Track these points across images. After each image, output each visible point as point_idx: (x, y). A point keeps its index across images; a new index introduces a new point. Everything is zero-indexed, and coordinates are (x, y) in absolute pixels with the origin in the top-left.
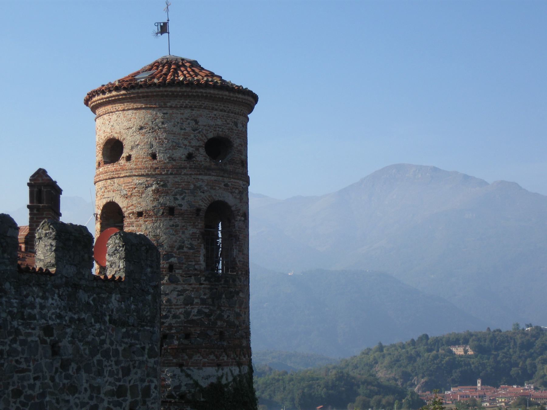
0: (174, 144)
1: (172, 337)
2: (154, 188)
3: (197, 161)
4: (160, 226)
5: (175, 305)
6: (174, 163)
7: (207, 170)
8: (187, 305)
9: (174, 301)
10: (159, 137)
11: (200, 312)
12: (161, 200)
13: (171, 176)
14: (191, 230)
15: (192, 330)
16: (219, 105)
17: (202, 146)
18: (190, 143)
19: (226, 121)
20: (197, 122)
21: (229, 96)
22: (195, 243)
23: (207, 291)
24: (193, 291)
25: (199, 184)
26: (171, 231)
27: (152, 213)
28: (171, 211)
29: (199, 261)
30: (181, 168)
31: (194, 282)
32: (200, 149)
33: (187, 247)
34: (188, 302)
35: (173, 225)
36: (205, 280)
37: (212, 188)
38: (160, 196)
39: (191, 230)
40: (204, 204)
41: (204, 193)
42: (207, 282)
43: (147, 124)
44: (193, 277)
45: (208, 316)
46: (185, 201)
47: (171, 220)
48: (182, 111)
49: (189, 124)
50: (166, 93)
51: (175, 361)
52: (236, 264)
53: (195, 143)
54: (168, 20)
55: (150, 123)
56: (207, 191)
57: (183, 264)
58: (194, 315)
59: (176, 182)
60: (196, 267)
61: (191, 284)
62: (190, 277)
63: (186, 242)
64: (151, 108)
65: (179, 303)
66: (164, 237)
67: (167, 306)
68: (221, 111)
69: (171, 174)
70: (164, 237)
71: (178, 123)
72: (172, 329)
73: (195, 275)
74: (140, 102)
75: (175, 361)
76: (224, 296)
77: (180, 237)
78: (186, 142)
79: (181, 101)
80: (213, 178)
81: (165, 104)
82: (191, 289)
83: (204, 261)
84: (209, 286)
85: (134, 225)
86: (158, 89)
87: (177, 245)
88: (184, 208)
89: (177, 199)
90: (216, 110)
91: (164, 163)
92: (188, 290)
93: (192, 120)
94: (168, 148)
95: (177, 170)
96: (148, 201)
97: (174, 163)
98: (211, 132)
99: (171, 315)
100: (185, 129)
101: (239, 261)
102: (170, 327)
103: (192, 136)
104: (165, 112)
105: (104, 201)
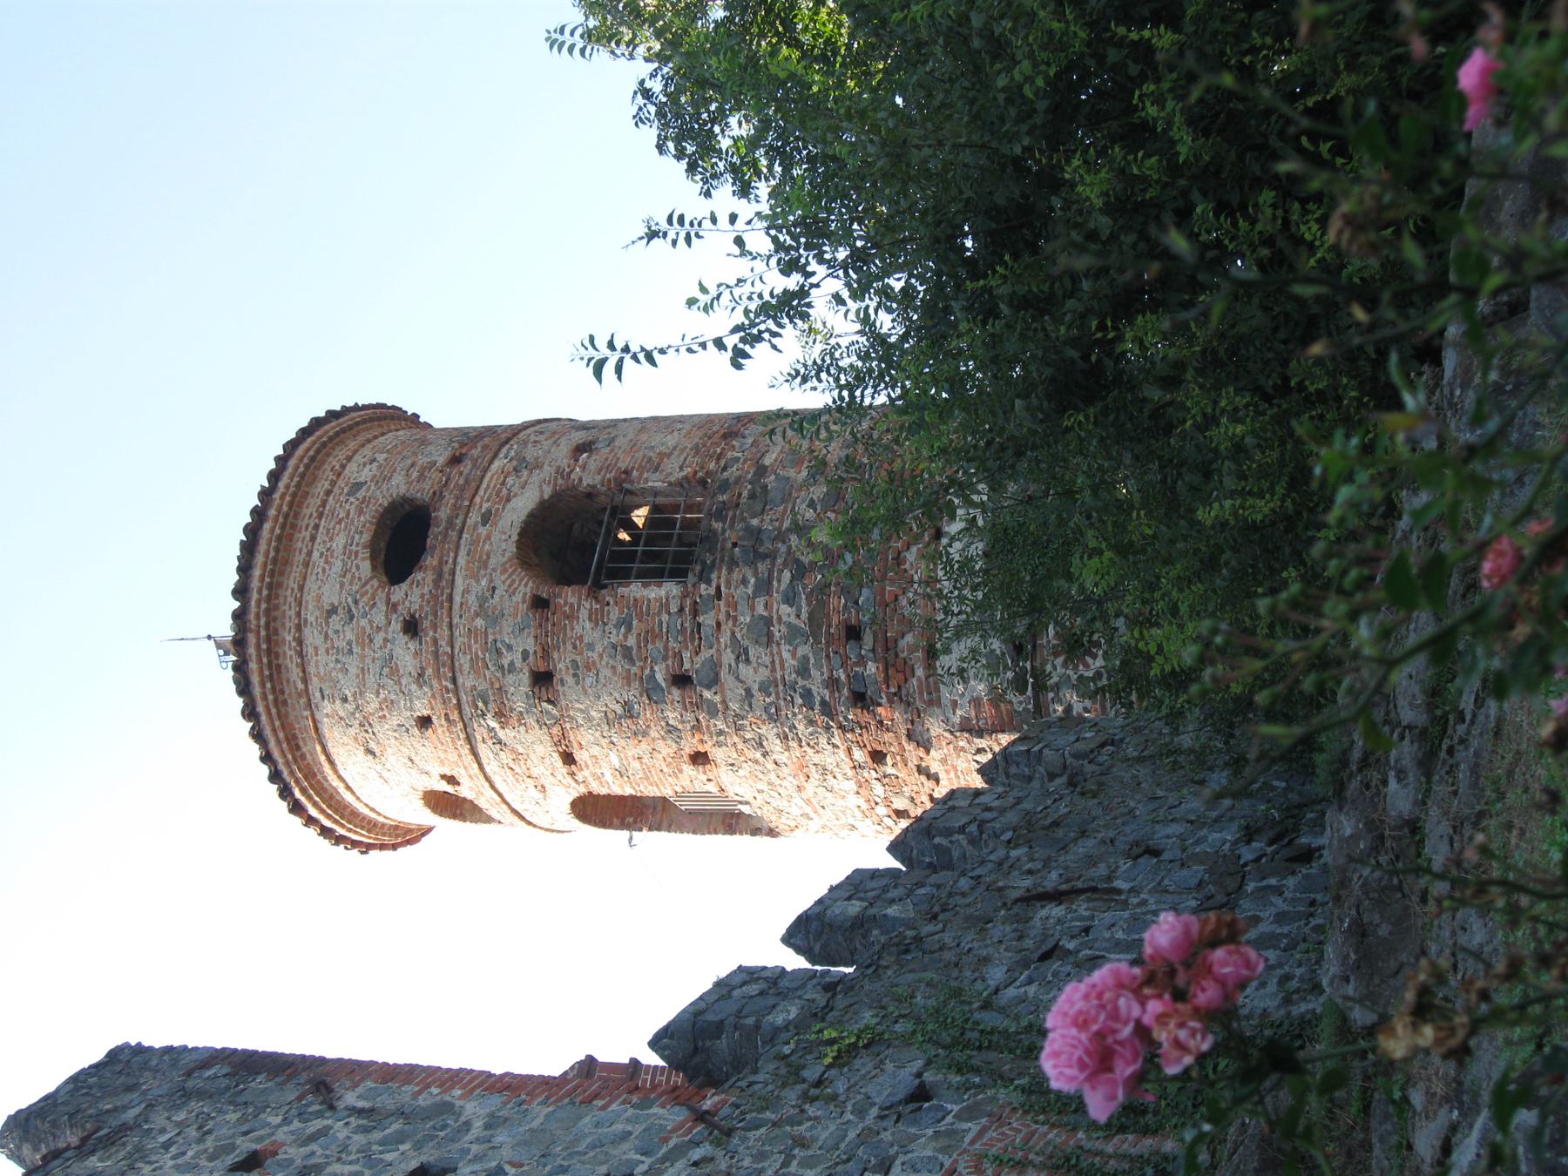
0: (386, 670)
1: (859, 678)
2: (493, 724)
3: (421, 607)
4: (582, 711)
5: (773, 670)
6: (429, 671)
7: (444, 579)
8: (770, 635)
9: (764, 673)
10: (377, 710)
11: (790, 599)
12: (520, 706)
13: (460, 681)
14: (584, 626)
15: (835, 621)
16: (299, 545)
17: (388, 594)
18: (379, 629)
19: (340, 522)
20: (333, 611)
21: (276, 519)
22: (614, 613)
23: (736, 576)
24: (735, 619)
25: (472, 600)
26: (589, 681)
27: (555, 730)
28: (543, 679)
29: (659, 600)
30: (436, 654)
31: (712, 613)
32: (394, 598)
33: (626, 637)
34: (764, 630)
35: (575, 675)
36: (709, 582)
37: (485, 565)
38: (512, 710)
39: (584, 626)
40: (522, 588)
41: (494, 589)
42: (714, 576)
43: (356, 739)
44: (701, 619)
45: (801, 571)
46: (513, 642)
47: (562, 682)
48: (311, 650)
49: (337, 632)
50: (271, 697)
51: (920, 672)
52: (686, 478)
53: (379, 617)
54: (209, 637)
55: (352, 731)
56: (491, 581)
57: (666, 648)
58: (798, 616)
59: (472, 667)
60: (674, 609)
61: (719, 625)
62: (699, 625)
63: (614, 639)
64: (316, 729)
65: (767, 660)
66: (606, 698)
67: (777, 694)
68: (313, 538)
69: (454, 680)
70: (606, 698)
71: (337, 661)
72: (837, 680)
73: (695, 613)
74: (313, 753)
75: (920, 672)
76: (755, 522)
77: (601, 656)
78: (379, 639)
79: (289, 653)
80: (462, 560)
81: (300, 695)
82: (730, 623)
83: (659, 585)
84: (724, 571)
85: (598, 772)
86: (264, 718)
87: (621, 665)
88: (530, 644)
89: (512, 663)
90: (310, 553)
91: (433, 696)
92: (733, 633)
93: (327, 624)
94: (397, 688)
95: (445, 667)
96: (530, 738)
97: (429, 671)
98: (358, 567)
99: (801, 682)
100: (349, 643)
101: (681, 468)
102: (832, 683)
103: (363, 622)
104: (318, 695)
105: (576, 823)
